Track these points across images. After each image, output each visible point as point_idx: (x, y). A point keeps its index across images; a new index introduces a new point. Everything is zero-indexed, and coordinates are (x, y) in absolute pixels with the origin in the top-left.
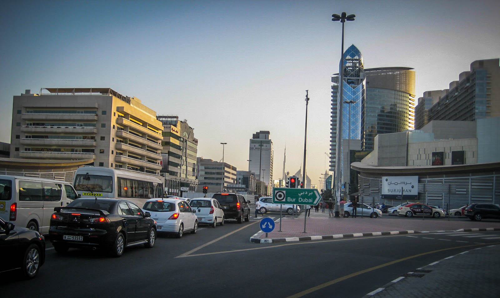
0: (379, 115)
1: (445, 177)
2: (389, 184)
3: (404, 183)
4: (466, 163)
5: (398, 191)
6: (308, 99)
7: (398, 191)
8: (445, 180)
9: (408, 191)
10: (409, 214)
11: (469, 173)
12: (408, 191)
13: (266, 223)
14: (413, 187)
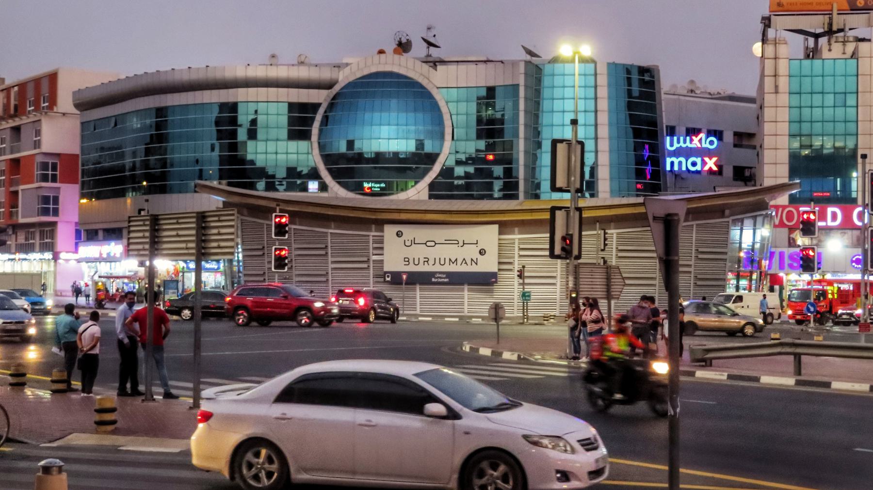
0: (218, 123)
1: (376, 231)
2: (408, 243)
3: (457, 242)
4: (803, 371)
5: (437, 261)
6: (758, 118)
7: (437, 261)
8: (373, 236)
9: (469, 262)
10: (571, 314)
11: (462, 284)
12: (469, 262)
13: (866, 221)
14: (482, 252)
